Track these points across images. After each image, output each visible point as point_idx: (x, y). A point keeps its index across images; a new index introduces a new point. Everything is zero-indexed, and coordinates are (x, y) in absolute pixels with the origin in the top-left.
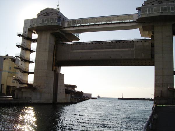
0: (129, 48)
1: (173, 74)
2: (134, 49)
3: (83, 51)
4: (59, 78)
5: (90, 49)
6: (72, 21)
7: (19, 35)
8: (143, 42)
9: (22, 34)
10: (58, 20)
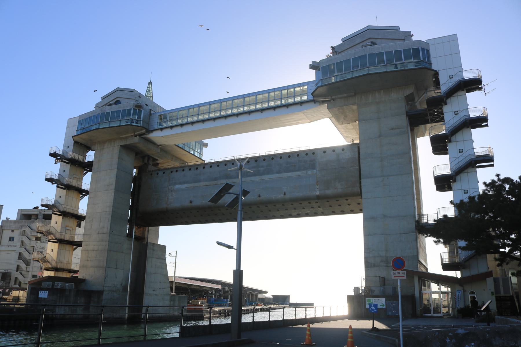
2: (315, 171)
4: (148, 255)
9: (60, 153)
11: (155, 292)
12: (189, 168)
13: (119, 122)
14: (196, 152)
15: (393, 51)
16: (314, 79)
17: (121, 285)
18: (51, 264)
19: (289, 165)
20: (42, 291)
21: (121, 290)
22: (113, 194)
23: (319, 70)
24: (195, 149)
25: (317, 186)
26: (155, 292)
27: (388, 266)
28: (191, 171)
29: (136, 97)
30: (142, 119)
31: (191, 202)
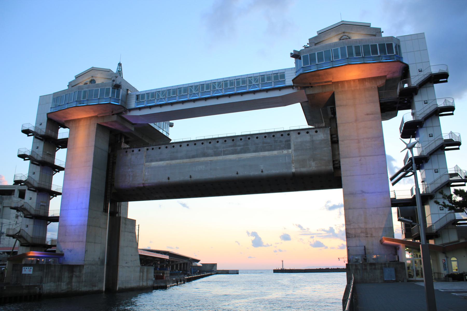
0: (280, 149)
1: (390, 204)
2: (290, 151)
3: (174, 162)
5: (189, 158)
6: (146, 96)
7: (27, 132)
8: (310, 133)
10: (113, 93)
11: (127, 265)
12: (166, 146)
13: (97, 101)
14: (164, 131)
15: (385, 44)
16: (294, 66)
17: (99, 258)
18: (26, 240)
19: (265, 145)
20: (26, 267)
21: (99, 264)
22: (91, 170)
23: (300, 59)
24: (163, 129)
25: (293, 164)
26: (127, 265)
27: (367, 237)
28: (167, 148)
29: (112, 77)
30: (120, 98)
31: (169, 179)
